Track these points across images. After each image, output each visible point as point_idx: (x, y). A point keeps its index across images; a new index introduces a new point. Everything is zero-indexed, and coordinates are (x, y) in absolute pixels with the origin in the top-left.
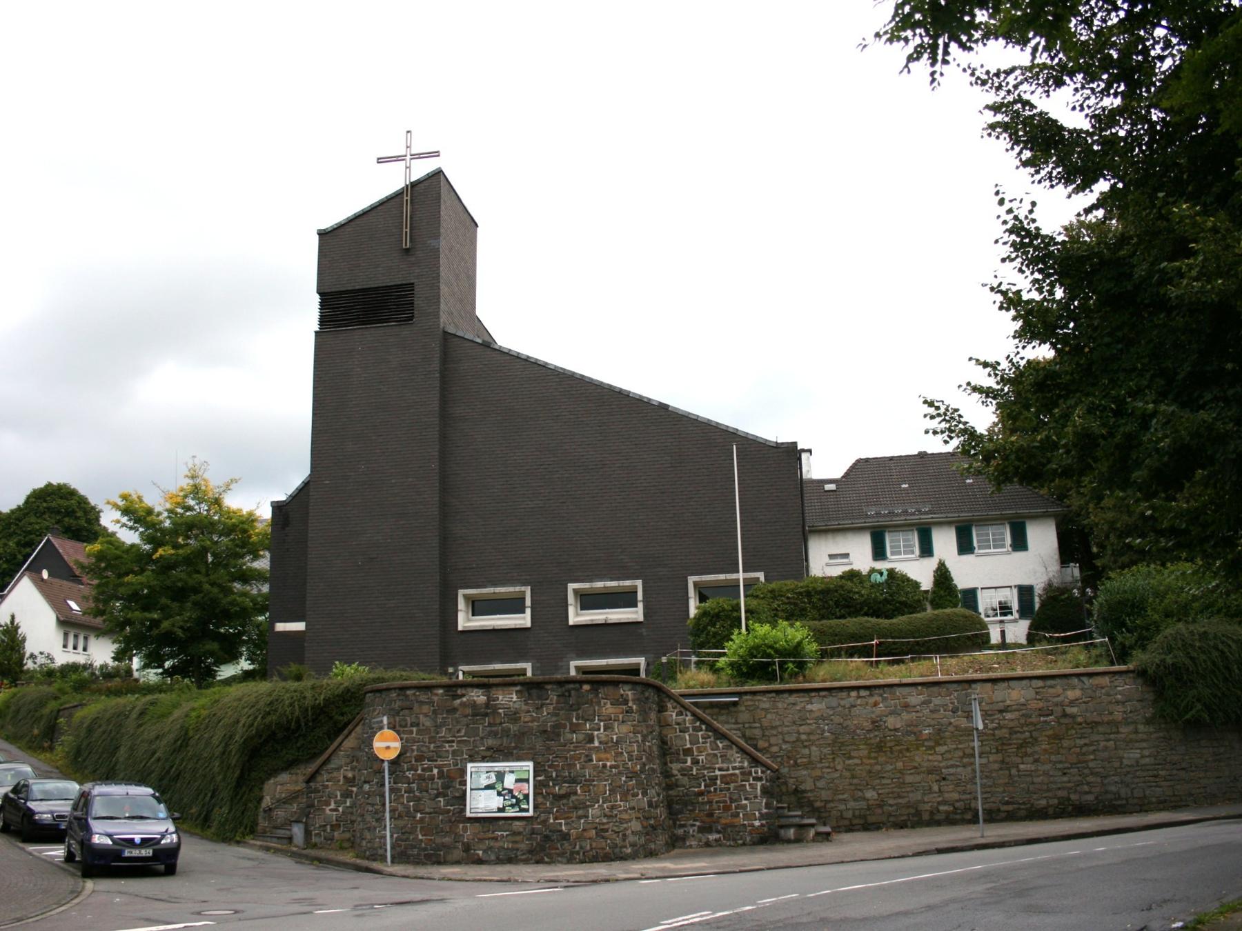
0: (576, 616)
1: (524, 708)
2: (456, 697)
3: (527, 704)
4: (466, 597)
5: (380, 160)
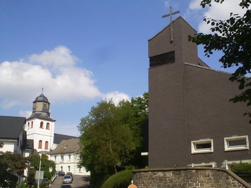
0: (227, 148)
1: (175, 178)
2: (155, 174)
3: (175, 177)
4: (227, 140)
5: (164, 17)
